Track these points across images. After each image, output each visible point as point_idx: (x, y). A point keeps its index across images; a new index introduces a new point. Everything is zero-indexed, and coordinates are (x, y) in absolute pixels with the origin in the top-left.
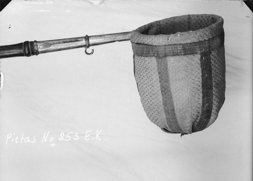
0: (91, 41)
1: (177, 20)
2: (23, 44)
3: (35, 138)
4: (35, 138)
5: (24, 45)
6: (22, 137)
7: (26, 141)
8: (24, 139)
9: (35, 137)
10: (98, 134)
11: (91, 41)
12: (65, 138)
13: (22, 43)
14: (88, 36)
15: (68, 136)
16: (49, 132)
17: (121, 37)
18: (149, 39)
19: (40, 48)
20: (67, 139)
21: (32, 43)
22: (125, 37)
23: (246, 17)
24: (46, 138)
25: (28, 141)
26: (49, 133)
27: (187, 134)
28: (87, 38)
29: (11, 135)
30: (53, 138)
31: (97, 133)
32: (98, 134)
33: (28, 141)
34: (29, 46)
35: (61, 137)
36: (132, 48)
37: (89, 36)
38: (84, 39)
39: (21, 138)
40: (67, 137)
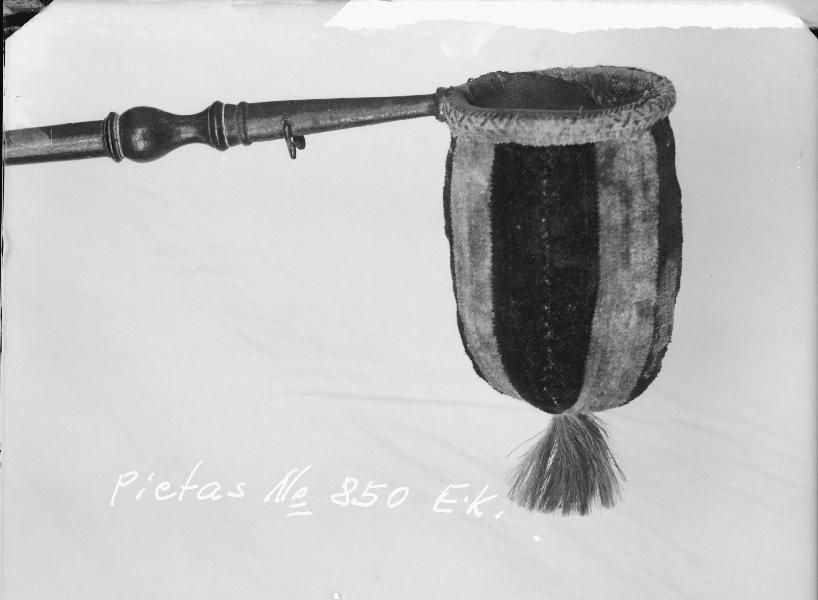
8: (197, 490)
15: (368, 492)
25: (120, 487)
30: (136, 474)
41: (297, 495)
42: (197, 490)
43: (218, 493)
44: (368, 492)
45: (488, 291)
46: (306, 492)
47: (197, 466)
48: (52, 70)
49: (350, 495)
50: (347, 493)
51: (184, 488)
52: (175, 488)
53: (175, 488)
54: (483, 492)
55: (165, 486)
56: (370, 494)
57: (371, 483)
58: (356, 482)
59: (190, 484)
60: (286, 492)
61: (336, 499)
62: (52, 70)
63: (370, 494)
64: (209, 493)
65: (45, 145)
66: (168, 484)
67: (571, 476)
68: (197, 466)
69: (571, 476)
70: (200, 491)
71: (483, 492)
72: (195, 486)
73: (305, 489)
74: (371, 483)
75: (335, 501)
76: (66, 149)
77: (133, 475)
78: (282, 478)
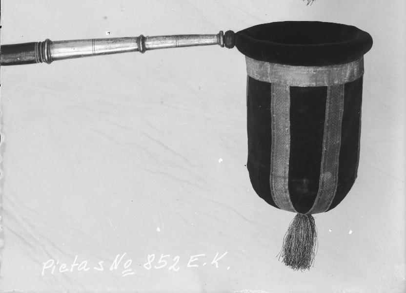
0: (149, 44)
2: (329, 92)
8: (78, 266)
10: (216, 259)
15: (162, 260)
17: (170, 43)
18: (263, 42)
20: (159, 265)
21: (41, 45)
24: (115, 264)
25: (83, 269)
26: (123, 259)
27: (35, 62)
28: (142, 39)
29: (52, 261)
30: (131, 261)
31: (216, 257)
32: (216, 259)
33: (83, 269)
34: (121, 256)
36: (245, 63)
38: (216, 37)
39: (73, 263)
40: (160, 262)
42: (78, 266)
44: (162, 260)
49: (151, 263)
50: (149, 263)
51: (73, 266)
54: (216, 256)
55: (63, 266)
56: (163, 261)
57: (162, 255)
58: (53, 261)
59: (76, 263)
60: (129, 274)
61: (85, 263)
63: (163, 261)
64: (162, 263)
67: (299, 253)
69: (299, 253)
70: (79, 267)
71: (216, 256)
72: (78, 264)
74: (162, 255)
75: (129, 261)
78: (114, 260)
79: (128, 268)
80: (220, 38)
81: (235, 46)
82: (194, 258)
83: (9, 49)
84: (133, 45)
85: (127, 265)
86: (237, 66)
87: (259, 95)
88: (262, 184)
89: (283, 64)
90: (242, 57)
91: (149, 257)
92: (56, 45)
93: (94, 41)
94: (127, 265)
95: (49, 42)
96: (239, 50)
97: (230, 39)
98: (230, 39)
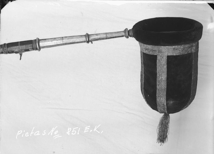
0: (91, 38)
1: (164, 79)
3: (45, 132)
4: (45, 132)
5: (7, 45)
6: (32, 132)
7: (35, 134)
8: (34, 133)
9: (45, 131)
11: (91, 38)
12: (71, 132)
13: (18, 42)
14: (89, 34)
15: (74, 130)
16: (57, 127)
18: (149, 31)
19: (123, 34)
22: (57, 42)
23: (20, 60)
28: (88, 36)
29: (35, 134)
30: (28, 133)
35: (68, 131)
37: (40, 40)
39: (31, 132)
40: (73, 131)
41: (55, 133)
43: (39, 133)
44: (74, 130)
45: (157, 68)
46: (58, 132)
47: (76, 128)
48: (14, 22)
52: (29, 134)
53: (29, 134)
56: (74, 131)
62: (14, 22)
63: (74, 131)
65: (60, 42)
66: (28, 133)
68: (76, 128)
73: (57, 131)
74: (69, 128)
76: (50, 45)
77: (21, 132)
79: (57, 134)
80: (86, 37)
81: (208, 28)
82: (87, 128)
83: (8, 48)
84: (84, 39)
85: (19, 133)
86: (133, 47)
87: (149, 62)
88: (152, 101)
89: (161, 46)
90: (137, 43)
91: (69, 129)
92: (92, 35)
93: (62, 38)
94: (19, 133)
95: (39, 40)
96: (136, 40)
97: (127, 33)
98: (127, 33)
